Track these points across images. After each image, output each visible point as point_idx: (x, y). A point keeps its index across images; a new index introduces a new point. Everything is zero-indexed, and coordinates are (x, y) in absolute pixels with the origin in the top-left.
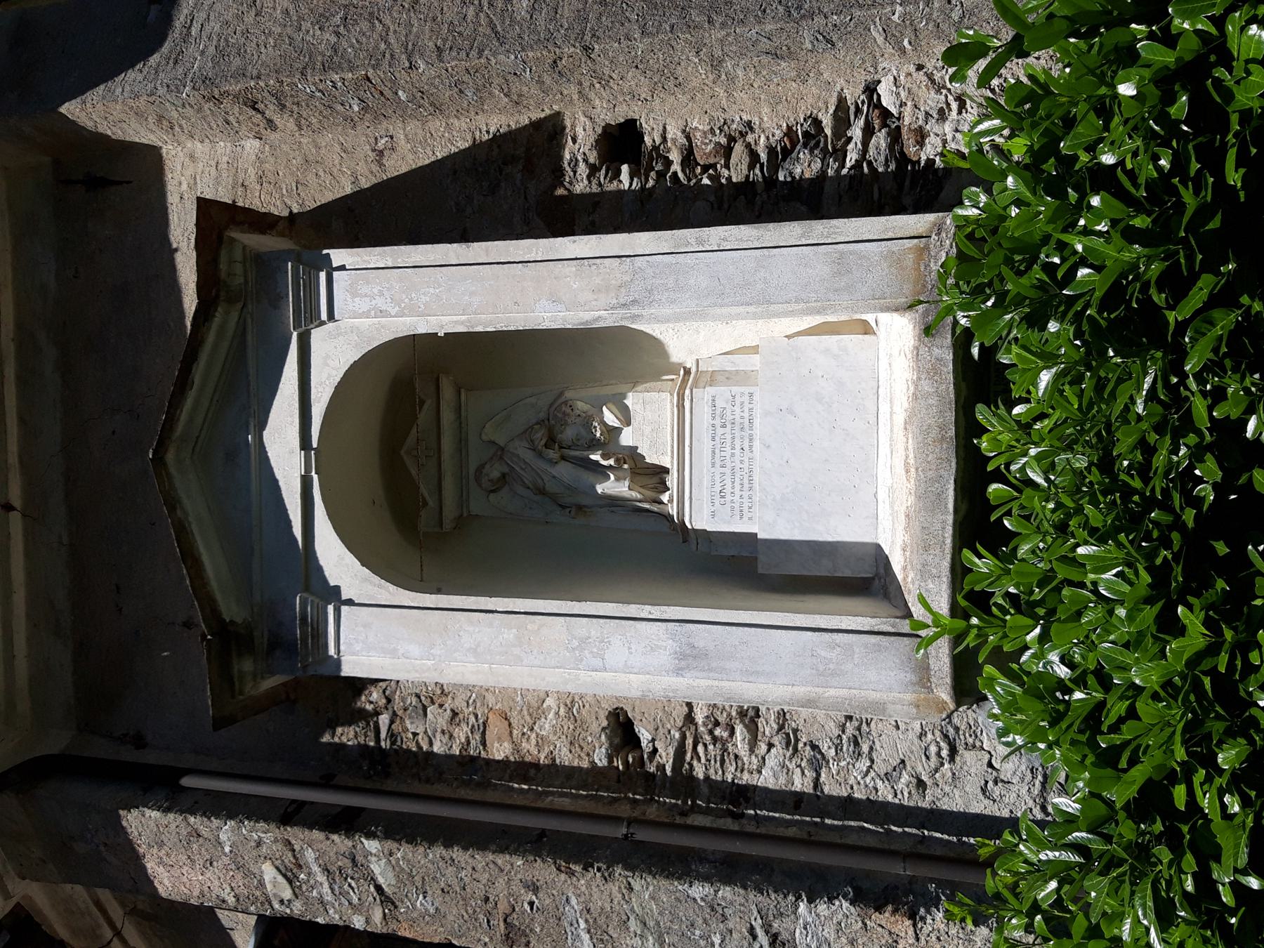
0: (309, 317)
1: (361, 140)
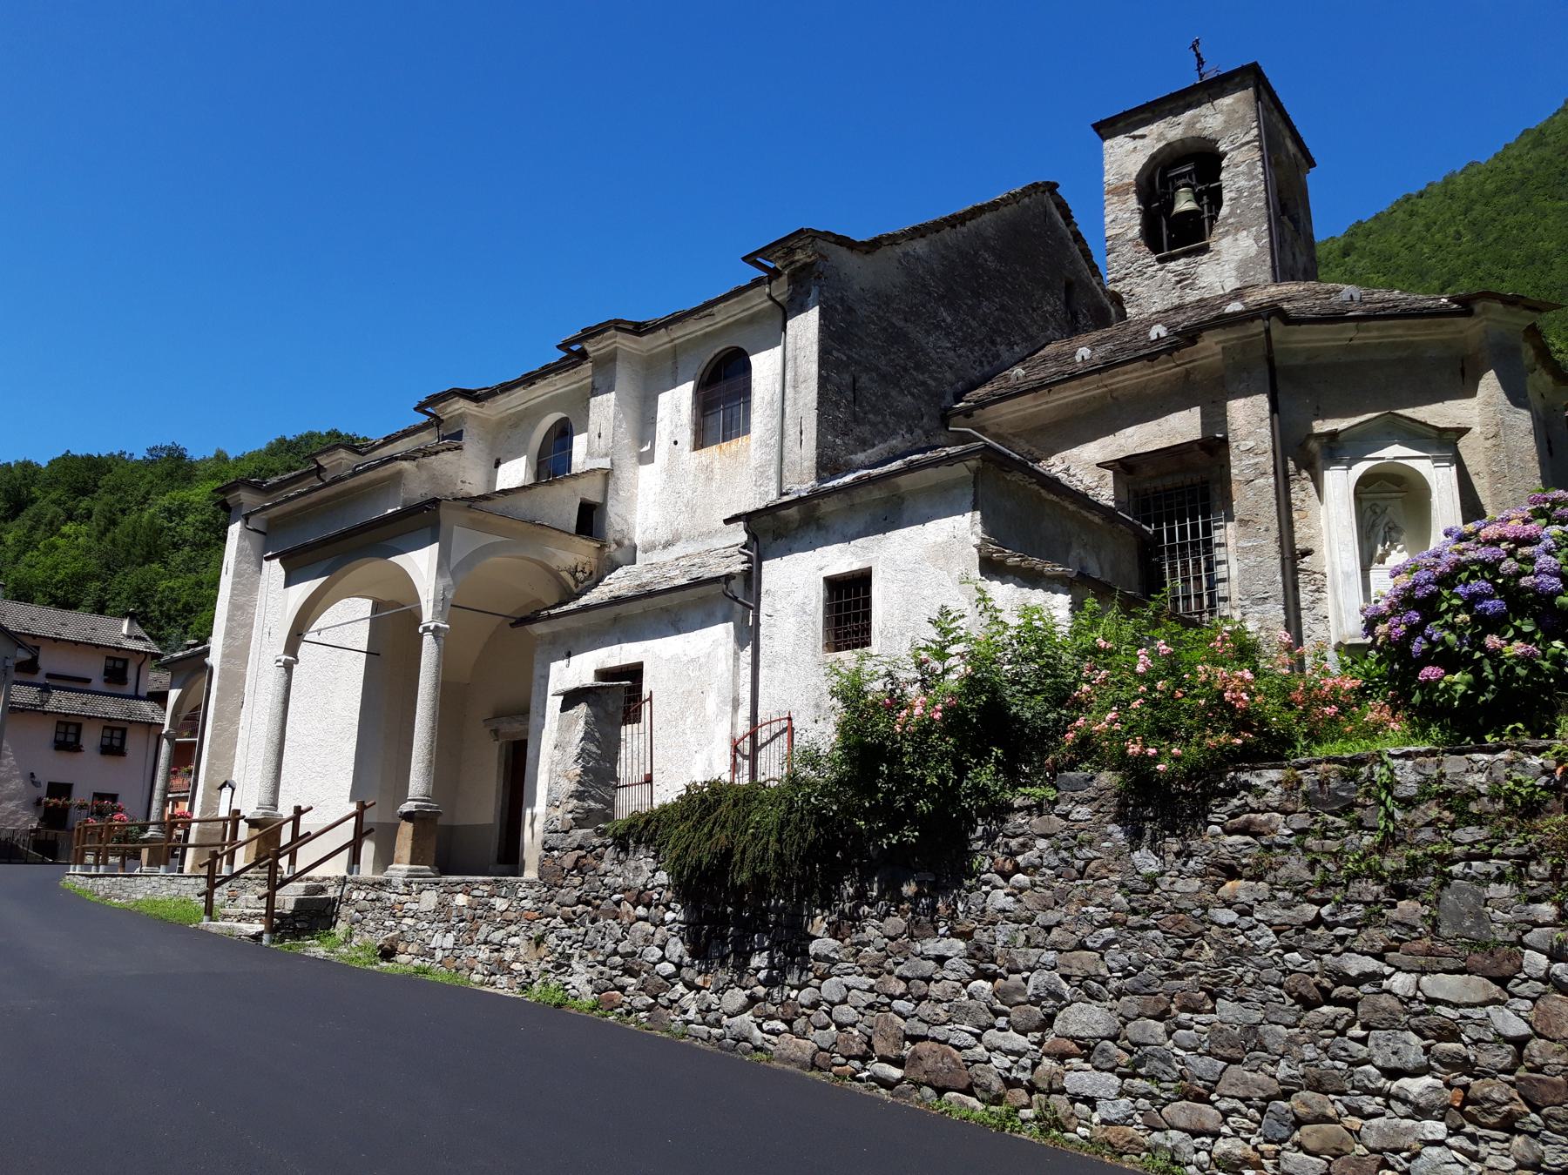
0: (1436, 460)
1: (1482, 468)
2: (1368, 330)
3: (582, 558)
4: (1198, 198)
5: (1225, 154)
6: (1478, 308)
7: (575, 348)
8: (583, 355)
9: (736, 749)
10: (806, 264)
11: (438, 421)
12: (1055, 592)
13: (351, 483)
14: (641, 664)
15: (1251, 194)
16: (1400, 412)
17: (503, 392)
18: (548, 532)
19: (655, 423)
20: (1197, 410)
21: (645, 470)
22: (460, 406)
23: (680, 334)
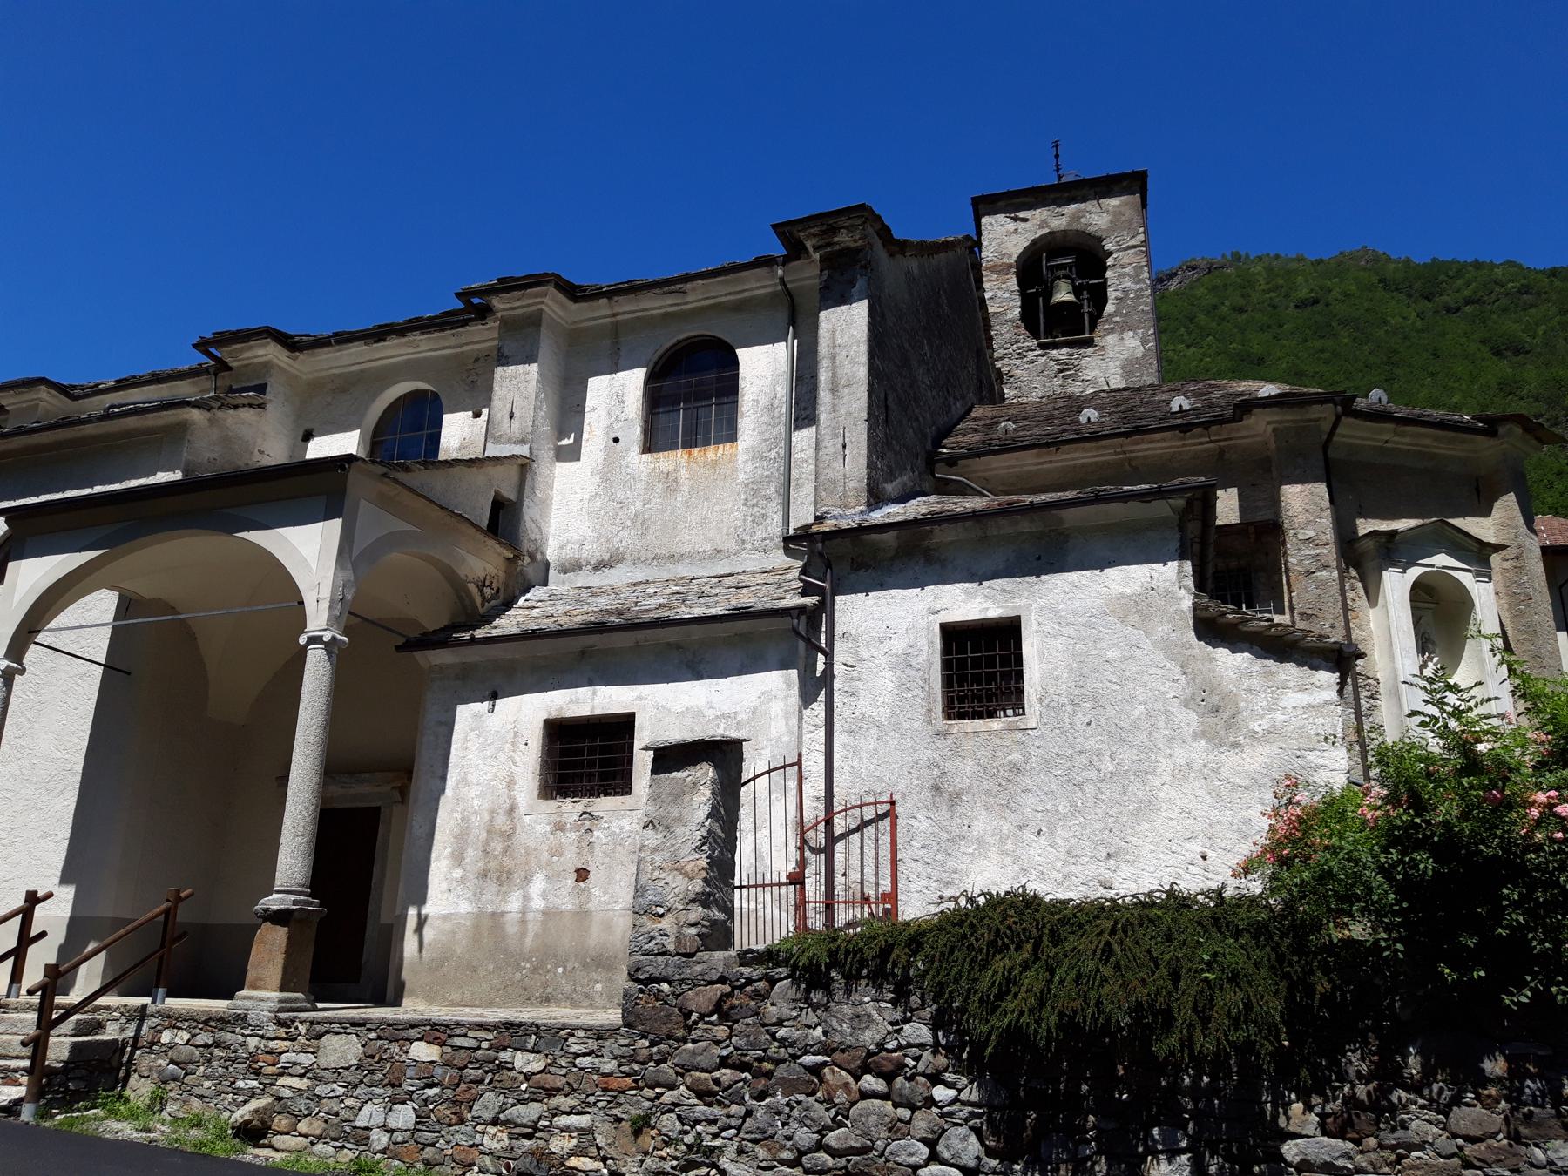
2: (1403, 434)
3: (491, 570)
4: (1077, 291)
5: (1111, 253)
6: (1502, 430)
7: (476, 301)
8: (484, 313)
9: (803, 844)
10: (848, 249)
11: (223, 368)
12: (1315, 668)
13: (89, 430)
14: (632, 715)
15: (1137, 297)
16: (1457, 522)
17: (338, 342)
18: (464, 527)
19: (582, 413)
20: (1235, 490)
21: (563, 469)
22: (270, 352)
23: (627, 308)
